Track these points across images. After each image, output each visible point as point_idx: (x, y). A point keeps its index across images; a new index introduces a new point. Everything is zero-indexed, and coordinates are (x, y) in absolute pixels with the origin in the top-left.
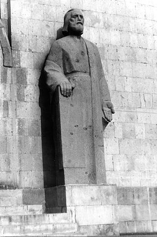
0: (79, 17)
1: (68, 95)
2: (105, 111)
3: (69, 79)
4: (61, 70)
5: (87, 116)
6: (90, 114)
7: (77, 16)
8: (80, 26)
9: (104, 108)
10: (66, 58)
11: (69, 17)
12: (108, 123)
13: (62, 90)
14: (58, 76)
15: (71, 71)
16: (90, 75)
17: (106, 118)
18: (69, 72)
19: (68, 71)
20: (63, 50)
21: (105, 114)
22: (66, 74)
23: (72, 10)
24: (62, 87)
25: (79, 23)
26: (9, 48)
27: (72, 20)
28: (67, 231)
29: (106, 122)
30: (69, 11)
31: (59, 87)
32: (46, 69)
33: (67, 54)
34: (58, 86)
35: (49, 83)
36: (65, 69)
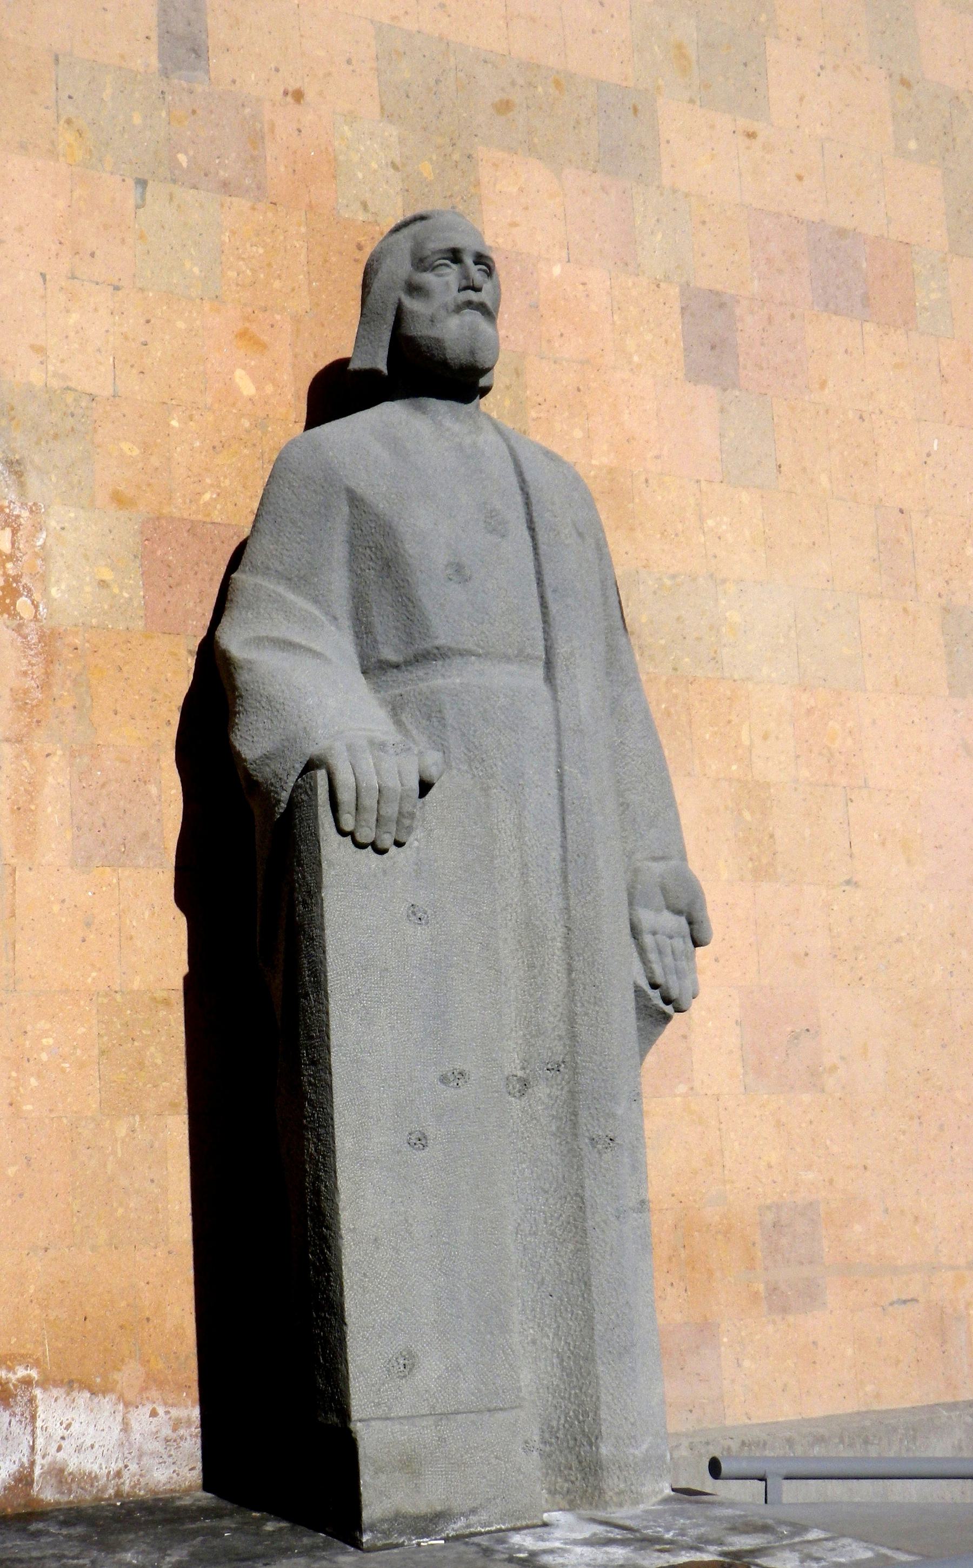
0: (469, 260)
1: (387, 841)
2: (648, 940)
3: (395, 709)
4: (339, 643)
5: (360, 730)
6: (556, 967)
7: (455, 256)
8: (474, 330)
9: (647, 918)
10: (379, 562)
11: (398, 267)
12: (667, 1018)
13: (346, 796)
14: (316, 700)
15: (411, 652)
16: (550, 677)
17: (654, 986)
18: (396, 651)
19: (389, 654)
20: (355, 500)
21: (653, 956)
22: (374, 668)
23: (422, 218)
24: (345, 778)
25: (469, 304)
26: (601, 1514)
27: (414, 289)
28: (70, 1561)
29: (659, 1006)
30: (397, 229)
31: (321, 776)
32: (233, 641)
33: (387, 530)
34: (311, 765)
35: (253, 741)
36: (363, 631)
